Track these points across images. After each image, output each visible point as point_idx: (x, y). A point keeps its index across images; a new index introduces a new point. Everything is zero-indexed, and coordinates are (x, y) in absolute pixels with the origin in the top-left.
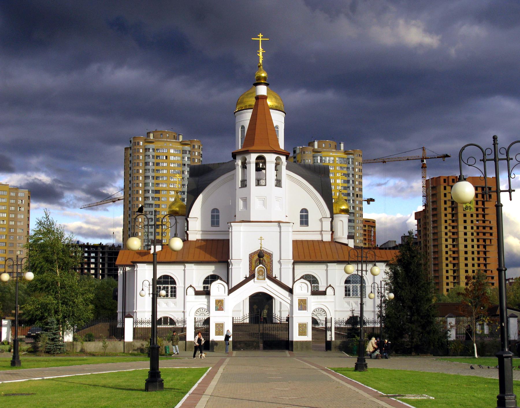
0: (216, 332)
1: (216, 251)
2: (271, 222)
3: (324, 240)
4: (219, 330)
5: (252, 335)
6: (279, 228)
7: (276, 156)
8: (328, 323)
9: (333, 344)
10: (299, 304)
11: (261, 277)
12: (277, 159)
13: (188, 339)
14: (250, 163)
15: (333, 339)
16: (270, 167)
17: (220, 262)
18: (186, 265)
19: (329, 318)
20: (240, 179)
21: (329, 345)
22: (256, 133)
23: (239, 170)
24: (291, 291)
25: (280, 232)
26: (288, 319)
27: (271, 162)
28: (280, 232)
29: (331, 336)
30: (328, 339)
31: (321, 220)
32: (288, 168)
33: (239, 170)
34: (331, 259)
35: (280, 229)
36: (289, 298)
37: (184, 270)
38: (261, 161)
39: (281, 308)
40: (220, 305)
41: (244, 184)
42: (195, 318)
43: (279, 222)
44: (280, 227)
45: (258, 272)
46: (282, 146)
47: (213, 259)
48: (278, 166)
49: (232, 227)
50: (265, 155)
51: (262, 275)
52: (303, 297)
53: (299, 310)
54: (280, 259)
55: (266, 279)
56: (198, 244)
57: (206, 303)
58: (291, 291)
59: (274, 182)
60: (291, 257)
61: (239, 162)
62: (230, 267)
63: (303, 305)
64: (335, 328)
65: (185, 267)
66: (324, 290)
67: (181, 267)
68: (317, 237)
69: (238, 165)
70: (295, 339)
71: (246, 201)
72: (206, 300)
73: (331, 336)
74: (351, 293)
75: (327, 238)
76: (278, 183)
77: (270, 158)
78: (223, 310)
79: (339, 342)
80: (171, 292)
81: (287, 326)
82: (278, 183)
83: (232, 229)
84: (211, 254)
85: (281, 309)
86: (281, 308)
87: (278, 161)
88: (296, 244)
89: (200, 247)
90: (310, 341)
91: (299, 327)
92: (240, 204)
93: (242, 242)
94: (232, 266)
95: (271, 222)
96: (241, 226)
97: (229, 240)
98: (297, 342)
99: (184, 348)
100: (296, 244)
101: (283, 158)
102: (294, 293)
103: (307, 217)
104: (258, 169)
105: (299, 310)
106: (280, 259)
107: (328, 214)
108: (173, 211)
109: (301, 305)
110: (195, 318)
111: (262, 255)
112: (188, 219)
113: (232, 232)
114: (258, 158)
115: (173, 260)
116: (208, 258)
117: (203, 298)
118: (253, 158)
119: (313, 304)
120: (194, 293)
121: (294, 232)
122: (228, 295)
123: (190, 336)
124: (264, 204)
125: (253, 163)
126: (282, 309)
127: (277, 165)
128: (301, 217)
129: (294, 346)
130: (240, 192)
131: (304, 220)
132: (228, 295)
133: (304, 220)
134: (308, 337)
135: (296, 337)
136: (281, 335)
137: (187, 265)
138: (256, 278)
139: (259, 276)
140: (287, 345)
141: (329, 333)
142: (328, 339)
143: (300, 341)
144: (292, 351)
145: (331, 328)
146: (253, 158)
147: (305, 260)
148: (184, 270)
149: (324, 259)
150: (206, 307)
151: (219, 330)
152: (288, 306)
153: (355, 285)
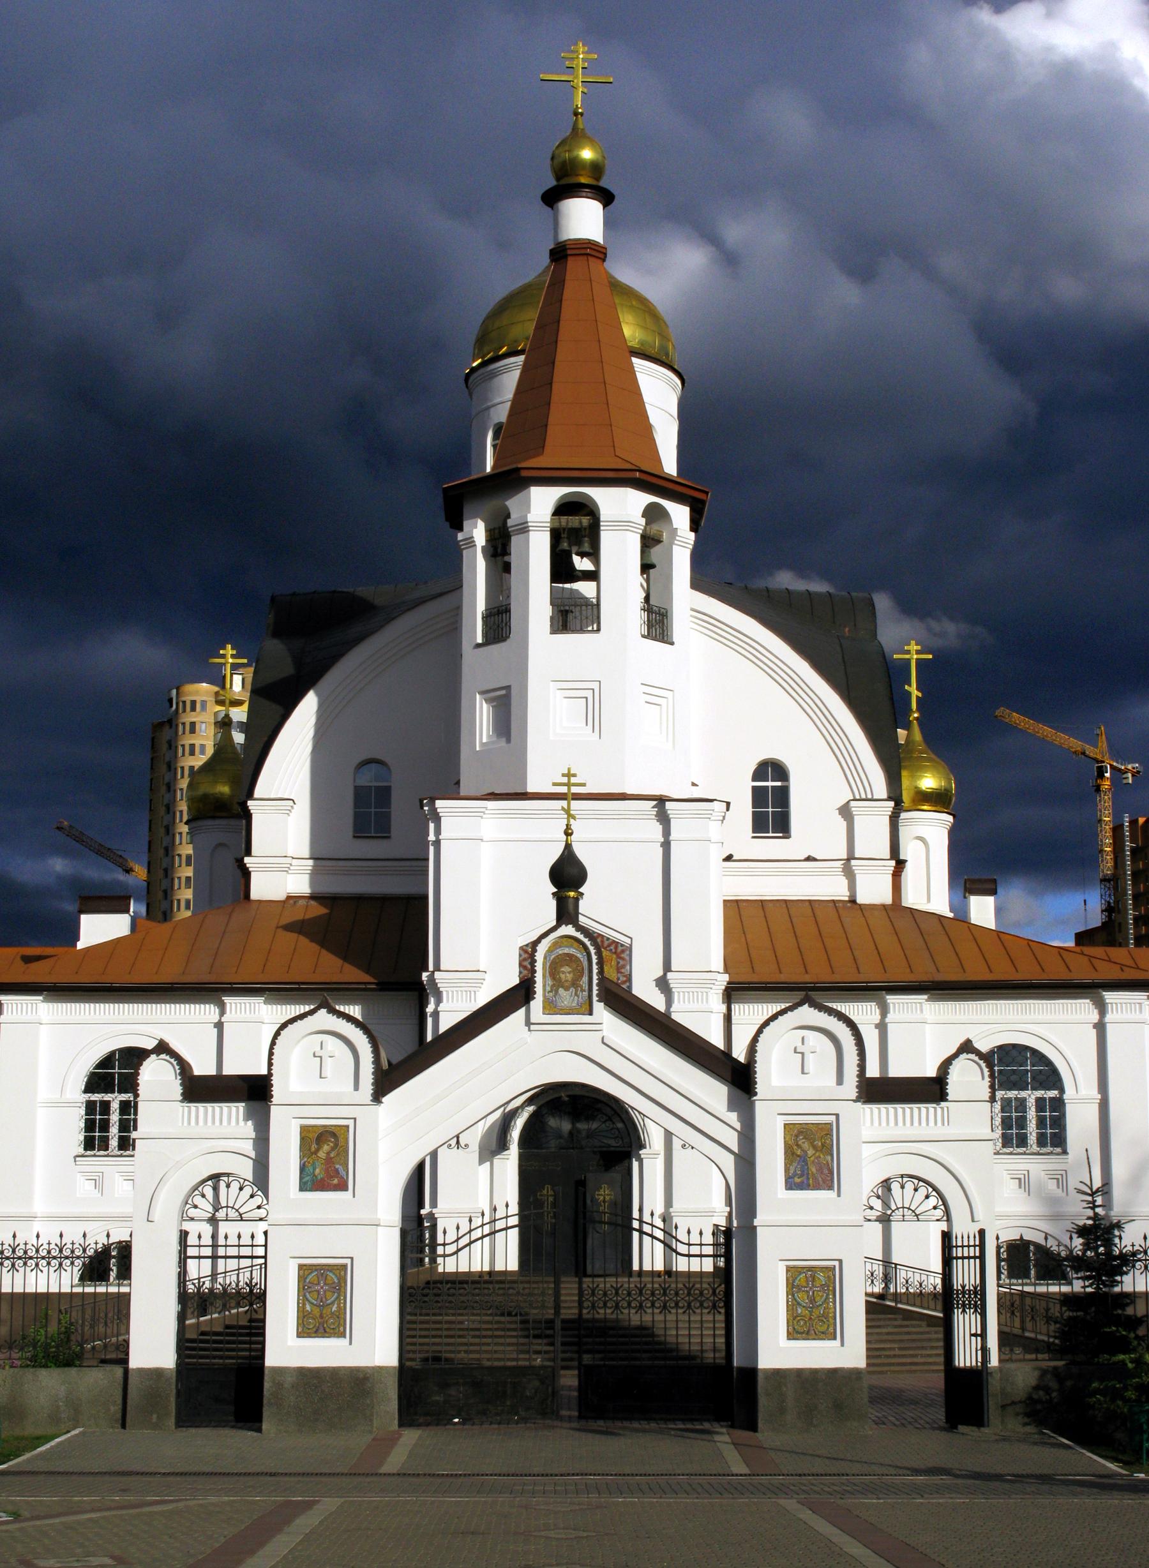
0: (789, 1333)
1: (371, 947)
2: (623, 797)
3: (861, 899)
4: (322, 1305)
5: (541, 1330)
6: (659, 828)
7: (648, 499)
8: (958, 1266)
9: (994, 1384)
10: (791, 1153)
11: (566, 997)
12: (653, 514)
13: (137, 1361)
14: (524, 529)
15: (994, 1361)
16: (620, 549)
17: (384, 986)
18: (228, 1000)
19: (963, 1229)
20: (481, 606)
21: (965, 1395)
22: (555, 398)
23: (479, 569)
24: (740, 1078)
25: (666, 845)
26: (725, 1239)
27: (623, 525)
28: (666, 845)
29: (975, 1341)
30: (966, 1356)
31: (845, 812)
32: (696, 585)
33: (479, 569)
34: (903, 976)
35: (667, 832)
36: (733, 1118)
37: (219, 1026)
38: (576, 532)
39: (669, 1202)
40: (329, 1161)
41: (501, 622)
42: (184, 1235)
43: (661, 801)
44: (664, 819)
45: (553, 970)
46: (670, 465)
47: (353, 974)
48: (656, 553)
49: (437, 819)
50: (597, 494)
51: (575, 984)
52: (813, 1113)
53: (790, 1185)
54: (667, 967)
55: (599, 1007)
56: (288, 918)
57: (248, 1147)
58: (740, 1078)
59: (636, 618)
60: (715, 957)
61: (478, 532)
62: (430, 1008)
63: (813, 1157)
64: (1000, 1297)
65: (222, 1013)
66: (932, 1072)
67: (207, 1012)
68: (833, 888)
69: (470, 542)
70: (767, 1360)
71: (507, 707)
72: (248, 1129)
73: (975, 1341)
74: (1032, 1114)
75: (874, 889)
76: (658, 624)
77: (620, 508)
78: (342, 1186)
79: (1025, 1375)
80: (105, 1126)
81: (726, 1285)
82: (658, 624)
83: (438, 831)
84: (346, 954)
85: (678, 1197)
86: (669, 1202)
87: (655, 528)
88: (740, 915)
89: (299, 927)
90: (854, 1373)
91: (792, 1287)
92: (481, 718)
93: (484, 894)
94: (439, 1001)
95: (623, 797)
96: (481, 814)
97: (425, 898)
98: (778, 1374)
99: (115, 1409)
100: (740, 915)
101: (680, 514)
102: (760, 1088)
103: (782, 797)
104: (562, 571)
105: (790, 1185)
106: (667, 967)
107: (880, 788)
108: (205, 798)
109: (803, 1159)
110: (184, 1235)
111: (573, 871)
112: (250, 803)
113: (437, 843)
114: (564, 508)
115: (168, 974)
116: (332, 967)
117: (230, 1119)
118: (541, 502)
119: (867, 1151)
120: (177, 1090)
121: (726, 865)
122: (379, 1094)
123: (153, 1344)
124: (593, 716)
125: (540, 528)
126: (677, 1205)
127: (649, 541)
128: (759, 796)
129: (763, 1401)
130: (478, 665)
131: (772, 809)
132: (379, 1094)
133: (772, 809)
134: (847, 1350)
135: (777, 1349)
136: (691, 1332)
137: (230, 1001)
138: (537, 1004)
139: (555, 989)
140: (725, 1391)
141: (964, 1323)
142: (966, 1356)
143: (799, 1372)
144: (752, 1427)
145: (980, 1291)
146: (541, 502)
147: (782, 978)
148: (219, 1026)
149: (871, 973)
150: (245, 1169)
151: (322, 1305)
152: (728, 1163)
153: (1012, 1094)
